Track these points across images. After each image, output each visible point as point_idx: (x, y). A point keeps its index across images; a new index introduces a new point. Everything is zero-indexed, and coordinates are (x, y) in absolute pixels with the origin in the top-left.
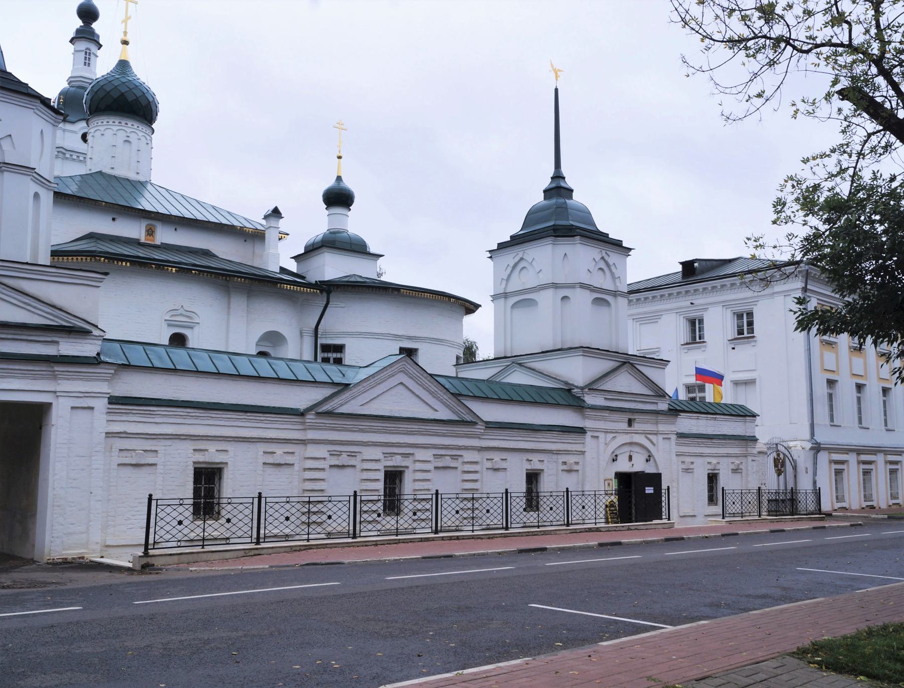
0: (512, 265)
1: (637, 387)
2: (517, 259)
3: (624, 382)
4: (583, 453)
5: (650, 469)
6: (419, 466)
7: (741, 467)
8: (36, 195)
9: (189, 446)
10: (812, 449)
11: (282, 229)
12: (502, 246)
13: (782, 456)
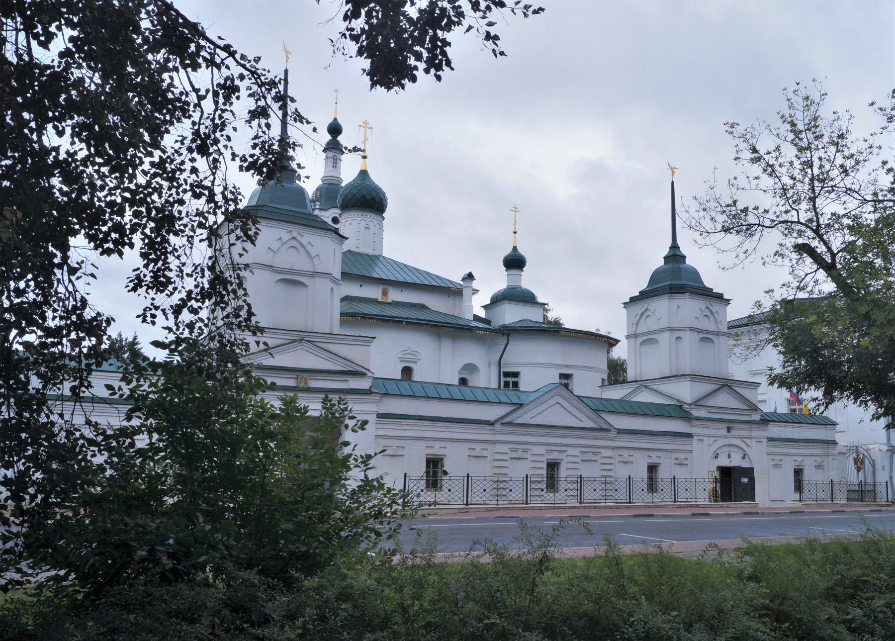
0: (640, 314)
1: (734, 403)
2: (643, 310)
3: (724, 400)
4: (691, 451)
5: (745, 464)
6: (570, 459)
7: (823, 464)
8: (332, 289)
9: (423, 444)
10: (888, 450)
11: (475, 287)
12: (633, 300)
13: (861, 456)
